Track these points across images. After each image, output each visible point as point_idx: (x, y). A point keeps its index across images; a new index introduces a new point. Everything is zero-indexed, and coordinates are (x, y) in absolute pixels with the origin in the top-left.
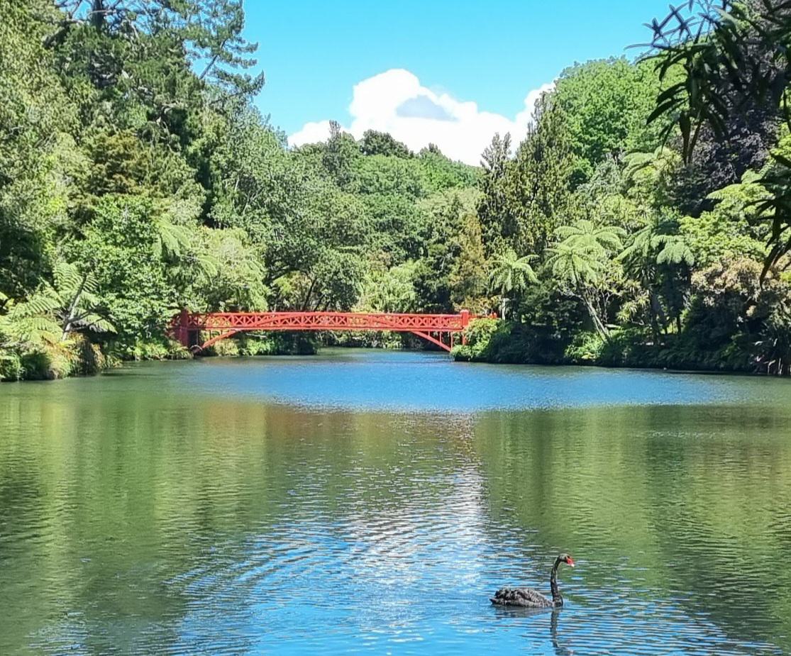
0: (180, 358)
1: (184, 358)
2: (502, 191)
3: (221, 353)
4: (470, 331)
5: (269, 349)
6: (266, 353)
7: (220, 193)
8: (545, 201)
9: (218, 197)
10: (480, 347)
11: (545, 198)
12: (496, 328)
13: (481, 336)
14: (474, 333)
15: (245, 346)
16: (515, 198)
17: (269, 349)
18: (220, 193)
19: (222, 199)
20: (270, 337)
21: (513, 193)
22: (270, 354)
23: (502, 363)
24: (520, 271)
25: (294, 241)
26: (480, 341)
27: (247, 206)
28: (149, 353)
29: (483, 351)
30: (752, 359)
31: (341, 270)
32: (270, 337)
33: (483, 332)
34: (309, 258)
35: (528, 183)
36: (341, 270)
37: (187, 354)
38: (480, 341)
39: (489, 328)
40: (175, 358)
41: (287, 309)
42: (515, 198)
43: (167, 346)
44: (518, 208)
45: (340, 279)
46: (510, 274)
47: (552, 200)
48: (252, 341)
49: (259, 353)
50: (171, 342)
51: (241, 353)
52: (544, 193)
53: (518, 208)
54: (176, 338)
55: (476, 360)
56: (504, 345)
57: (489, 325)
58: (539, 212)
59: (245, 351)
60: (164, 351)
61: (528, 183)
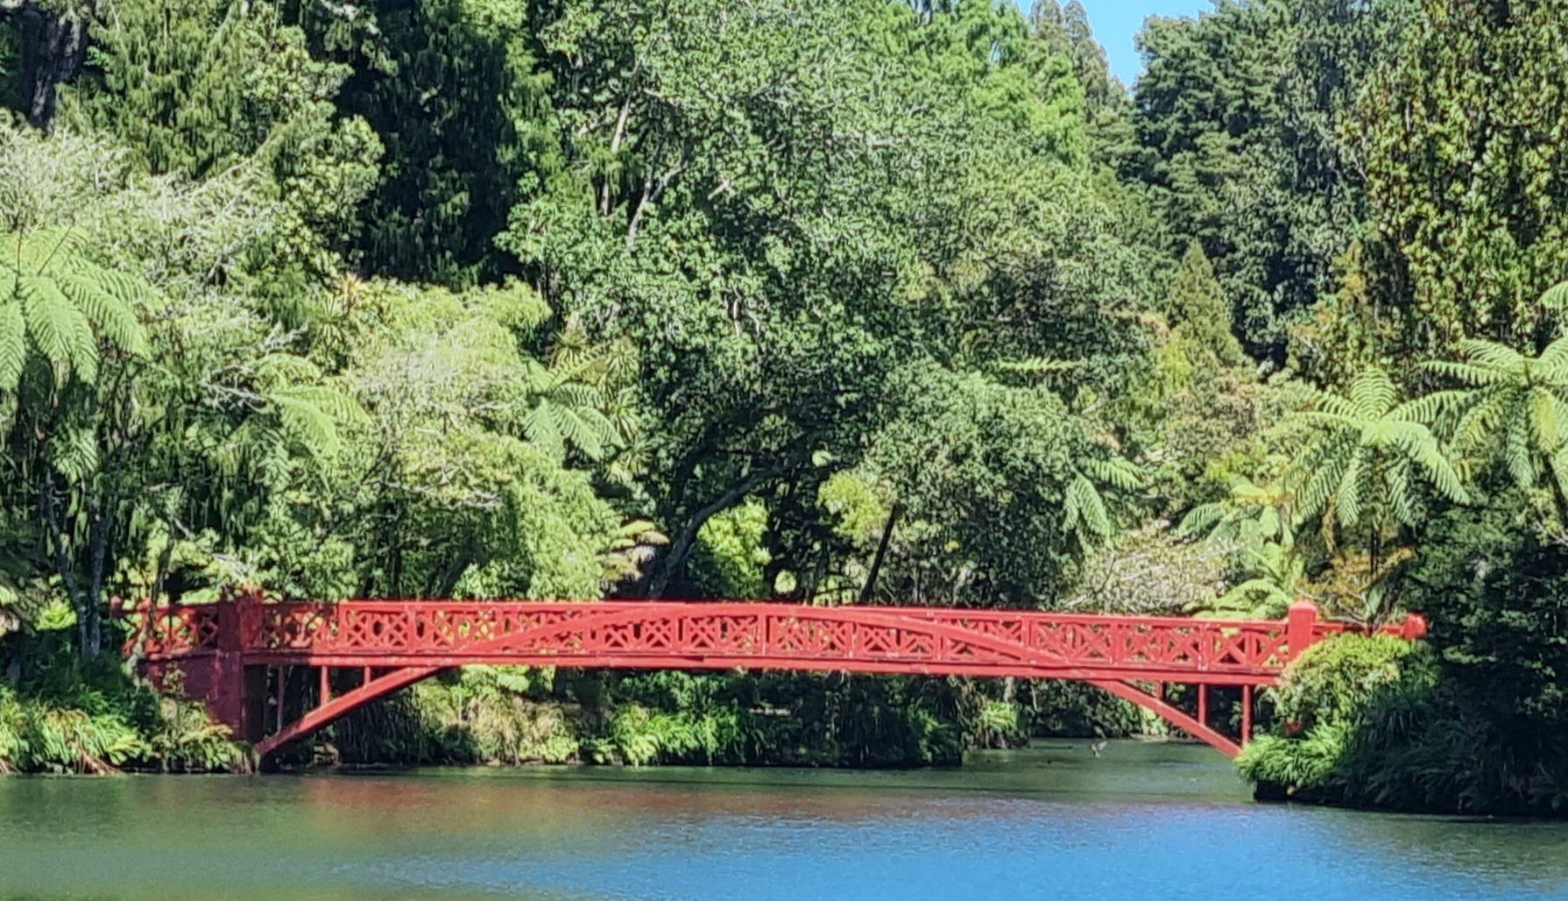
0: (199, 768)
1: (219, 769)
2: (1353, 141)
3: (499, 754)
4: (1297, 681)
5: (712, 744)
6: (697, 757)
7: (551, 159)
8: (1516, 183)
9: (543, 174)
10: (1327, 740)
11: (1514, 170)
12: (1393, 672)
13: (1334, 704)
14: (1308, 690)
15: (604, 730)
16: (1402, 171)
17: (712, 744)
18: (551, 159)
19: (559, 182)
20: (722, 697)
21: (1396, 155)
22: (717, 762)
23: (1386, 807)
24: (1395, 453)
25: (795, 340)
26: (1329, 721)
27: (646, 205)
28: (53, 749)
29: (1336, 762)
30: (796, 714)
31: (978, 450)
32: (722, 697)
33: (1341, 685)
34: (867, 402)
35: (1456, 113)
36: (978, 450)
37: (226, 753)
38: (1329, 721)
39: (1363, 670)
40: (178, 767)
41: (943, 607)
42: (1402, 171)
43: (145, 721)
44: (1411, 210)
45: (973, 483)
46: (1355, 463)
47: (1544, 178)
48: (641, 712)
49: (665, 757)
50: (168, 709)
51: (587, 755)
52: (1512, 152)
53: (1411, 210)
54: (192, 693)
55: (1314, 795)
56: (1400, 738)
57: (1365, 659)
58: (1492, 227)
59: (604, 747)
60: (125, 740)
61: (1456, 113)
